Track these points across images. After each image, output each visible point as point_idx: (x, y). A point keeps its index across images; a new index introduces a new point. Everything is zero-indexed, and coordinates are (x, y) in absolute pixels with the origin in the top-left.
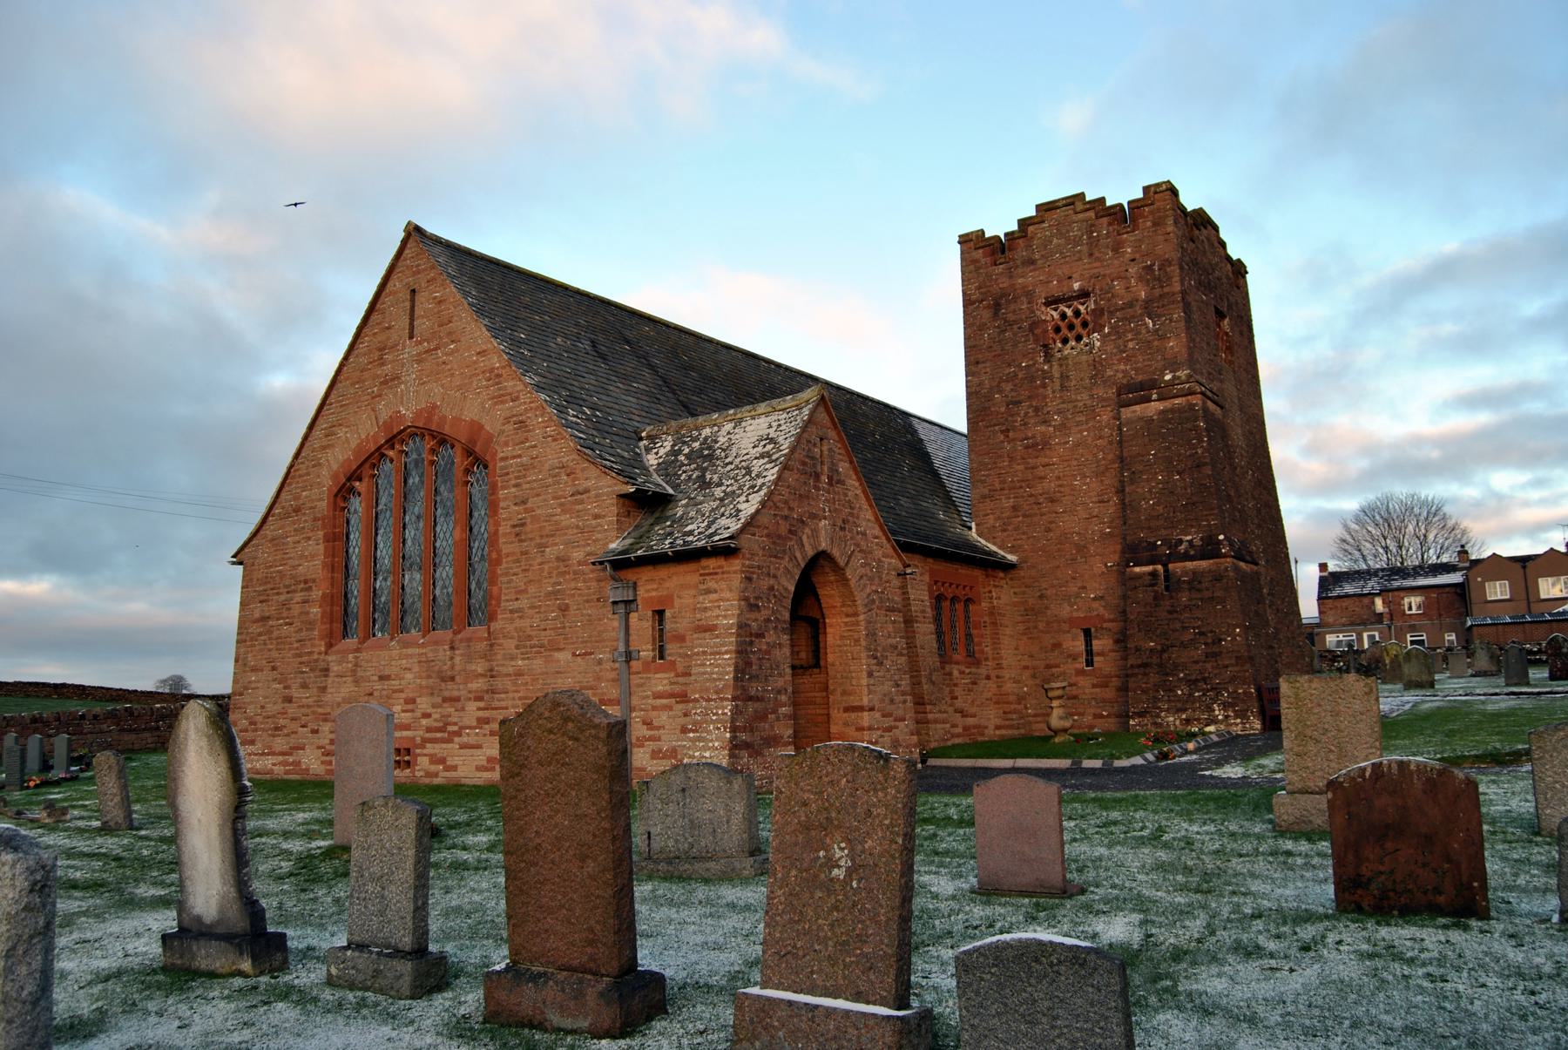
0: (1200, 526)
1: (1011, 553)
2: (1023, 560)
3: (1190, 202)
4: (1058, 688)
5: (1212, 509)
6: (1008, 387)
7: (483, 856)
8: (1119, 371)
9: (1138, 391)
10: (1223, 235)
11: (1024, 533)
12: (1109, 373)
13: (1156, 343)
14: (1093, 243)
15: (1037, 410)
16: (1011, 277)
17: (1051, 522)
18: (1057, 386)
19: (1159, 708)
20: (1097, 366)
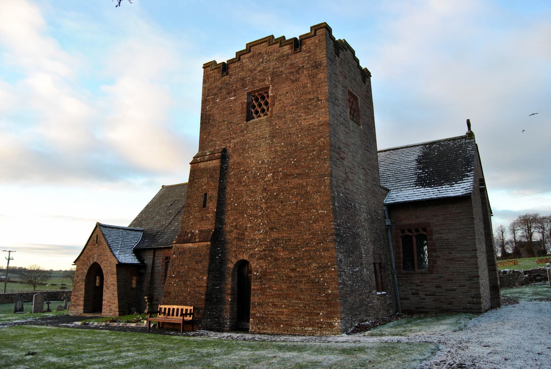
3: (337, 35)
7: (467, 141)
10: (357, 55)
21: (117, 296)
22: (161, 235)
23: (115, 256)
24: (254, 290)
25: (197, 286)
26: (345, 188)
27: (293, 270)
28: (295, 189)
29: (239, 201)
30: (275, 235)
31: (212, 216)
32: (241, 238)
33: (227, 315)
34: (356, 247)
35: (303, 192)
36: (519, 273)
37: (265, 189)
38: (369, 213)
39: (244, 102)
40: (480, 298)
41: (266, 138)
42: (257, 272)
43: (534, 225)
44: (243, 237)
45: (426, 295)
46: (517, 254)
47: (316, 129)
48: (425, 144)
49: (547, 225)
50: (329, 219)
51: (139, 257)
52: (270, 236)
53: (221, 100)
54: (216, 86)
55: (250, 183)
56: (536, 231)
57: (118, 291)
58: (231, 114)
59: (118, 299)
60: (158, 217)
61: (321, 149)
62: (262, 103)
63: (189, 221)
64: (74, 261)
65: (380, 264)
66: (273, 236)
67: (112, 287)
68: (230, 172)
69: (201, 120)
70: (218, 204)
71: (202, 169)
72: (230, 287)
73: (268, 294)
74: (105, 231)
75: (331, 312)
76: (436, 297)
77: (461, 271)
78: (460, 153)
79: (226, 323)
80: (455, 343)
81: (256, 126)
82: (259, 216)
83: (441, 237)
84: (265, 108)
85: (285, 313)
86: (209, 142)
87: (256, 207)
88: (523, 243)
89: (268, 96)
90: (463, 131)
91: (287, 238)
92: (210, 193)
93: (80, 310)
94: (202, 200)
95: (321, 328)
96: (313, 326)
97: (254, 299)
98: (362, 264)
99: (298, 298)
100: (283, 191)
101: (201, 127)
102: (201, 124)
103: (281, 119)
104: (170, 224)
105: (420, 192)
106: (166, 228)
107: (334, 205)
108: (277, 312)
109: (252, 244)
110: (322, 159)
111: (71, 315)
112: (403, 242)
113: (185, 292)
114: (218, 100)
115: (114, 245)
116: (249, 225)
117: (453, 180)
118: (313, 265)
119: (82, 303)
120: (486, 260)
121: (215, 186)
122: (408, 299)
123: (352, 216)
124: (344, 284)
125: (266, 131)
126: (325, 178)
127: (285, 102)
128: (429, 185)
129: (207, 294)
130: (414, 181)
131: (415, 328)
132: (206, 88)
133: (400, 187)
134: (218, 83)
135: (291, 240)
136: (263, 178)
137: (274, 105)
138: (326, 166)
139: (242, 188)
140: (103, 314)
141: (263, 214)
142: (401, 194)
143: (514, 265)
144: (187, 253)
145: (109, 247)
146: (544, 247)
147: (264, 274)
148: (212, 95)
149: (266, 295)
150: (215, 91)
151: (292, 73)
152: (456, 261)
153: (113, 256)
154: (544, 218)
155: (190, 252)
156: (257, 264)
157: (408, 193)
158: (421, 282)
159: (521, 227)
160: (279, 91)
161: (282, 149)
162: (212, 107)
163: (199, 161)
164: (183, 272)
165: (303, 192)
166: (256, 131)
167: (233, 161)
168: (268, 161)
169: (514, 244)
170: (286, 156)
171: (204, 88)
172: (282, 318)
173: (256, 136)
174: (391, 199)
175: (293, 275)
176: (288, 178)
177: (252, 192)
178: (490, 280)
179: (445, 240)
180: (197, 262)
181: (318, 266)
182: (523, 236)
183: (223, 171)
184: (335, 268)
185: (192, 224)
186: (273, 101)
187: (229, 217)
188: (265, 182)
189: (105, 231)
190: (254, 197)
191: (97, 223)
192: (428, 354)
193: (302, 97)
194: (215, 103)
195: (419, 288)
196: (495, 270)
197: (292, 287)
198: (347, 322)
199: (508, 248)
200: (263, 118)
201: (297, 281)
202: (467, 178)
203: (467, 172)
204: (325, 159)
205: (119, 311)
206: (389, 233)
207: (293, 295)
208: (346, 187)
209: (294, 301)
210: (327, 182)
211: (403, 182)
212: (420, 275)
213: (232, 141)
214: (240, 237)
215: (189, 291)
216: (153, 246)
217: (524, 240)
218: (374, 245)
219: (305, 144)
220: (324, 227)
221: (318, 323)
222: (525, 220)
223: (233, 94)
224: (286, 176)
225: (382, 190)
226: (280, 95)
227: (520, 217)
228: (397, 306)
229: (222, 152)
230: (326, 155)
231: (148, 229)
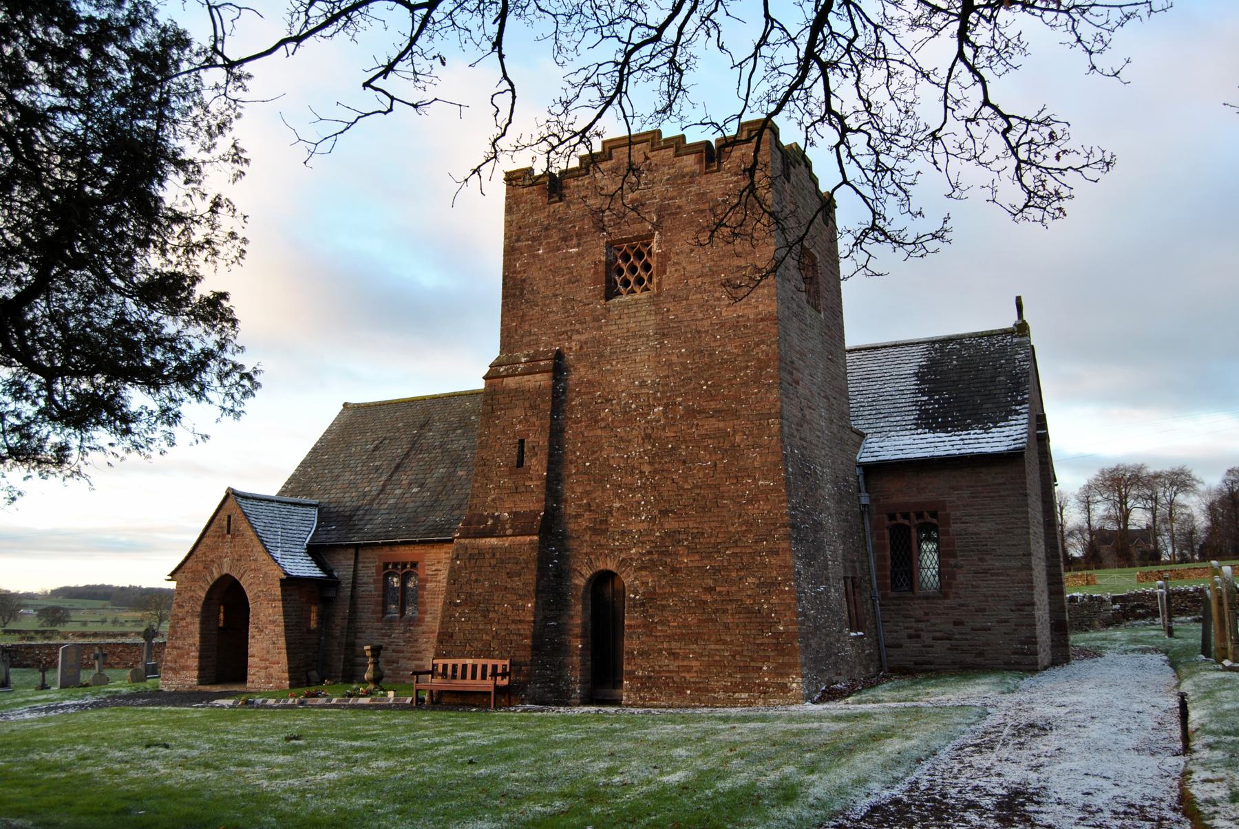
7: (1015, 340)
21: (284, 646)
22: (364, 515)
23: (276, 561)
24: (630, 626)
25: (513, 622)
26: (800, 439)
27: (710, 590)
28: (710, 438)
29: (595, 456)
30: (670, 524)
31: (537, 486)
32: (599, 528)
33: (575, 674)
34: (819, 548)
35: (727, 446)
36: (1101, 601)
37: (648, 437)
38: (836, 484)
39: (600, 261)
40: (1036, 643)
41: (648, 336)
43: (1134, 492)
44: (603, 527)
45: (934, 638)
46: (1093, 559)
47: (751, 326)
48: (932, 342)
49: (1164, 493)
50: (778, 496)
51: (320, 564)
52: (662, 525)
53: (549, 252)
54: (536, 221)
55: (615, 424)
56: (1138, 505)
57: (286, 637)
58: (570, 282)
59: (288, 653)
60: (347, 476)
61: (762, 365)
62: (638, 264)
63: (487, 494)
64: (169, 572)
65: (853, 578)
66: (666, 526)
67: (272, 627)
68: (572, 400)
69: (503, 288)
70: (550, 462)
71: (510, 391)
72: (579, 621)
73: (659, 634)
74: (247, 506)
75: (784, 665)
76: (953, 642)
77: (1000, 593)
78: (1002, 364)
79: (574, 691)
80: (1010, 705)
81: (626, 311)
82: (638, 487)
83: (965, 530)
84: (645, 277)
85: (695, 669)
86: (522, 336)
87: (630, 470)
88: (1107, 534)
89: (650, 253)
90: (1008, 320)
91: (696, 531)
92: (531, 439)
93: (190, 679)
94: (515, 452)
95: (765, 693)
96: (747, 689)
97: (632, 644)
98: (828, 579)
99: (720, 641)
100: (685, 441)
101: (503, 303)
102: (504, 297)
103: (679, 302)
104: (382, 491)
105: (925, 441)
106: (374, 500)
107: (786, 470)
108: (679, 667)
109: (623, 540)
110: (764, 385)
111: (166, 689)
112: (891, 538)
113: (487, 634)
114: (541, 252)
115: (268, 537)
116: (617, 505)
117: (990, 420)
118: (749, 580)
119: (194, 663)
120: (1045, 573)
121: (542, 426)
122: (901, 646)
123: (812, 490)
124: (805, 616)
125: (648, 323)
126: (770, 421)
127: (688, 268)
128: (943, 427)
129: (535, 637)
130: (912, 417)
131: (933, 690)
132: (514, 224)
133: (886, 429)
134: (541, 217)
135: (703, 533)
136: (644, 415)
137: (665, 272)
138: (771, 398)
139: (599, 432)
140: (248, 685)
141: (645, 484)
142: (889, 444)
143: (1087, 584)
144: (487, 556)
145: (262, 541)
146: (1156, 543)
147: (651, 597)
148: (528, 240)
149: (656, 637)
150: (534, 232)
151: (702, 211)
152: (992, 575)
153: (270, 561)
154: (1157, 476)
155: (494, 555)
156: (636, 579)
157: (902, 443)
158: (926, 614)
159: (1105, 496)
160: (674, 246)
161: (681, 360)
162: (528, 263)
163: (505, 373)
164: (480, 594)
165: (727, 446)
166: (626, 320)
167: (578, 377)
168: (652, 381)
169: (1087, 537)
170: (690, 374)
171: (508, 224)
172: (688, 678)
173: (628, 332)
174: (869, 454)
175: (708, 598)
176: (695, 417)
177: (622, 440)
178: (1051, 612)
179: (972, 534)
180: (510, 575)
181: (757, 582)
182: (1109, 518)
183: (557, 397)
184: (790, 586)
185: (493, 500)
186: (661, 263)
187: (572, 488)
188: (648, 422)
189: (247, 506)
190: (626, 450)
191: (229, 489)
192: (975, 719)
193: (722, 263)
194: (534, 256)
195: (921, 625)
196: (1062, 593)
197: (707, 621)
198: (810, 683)
199: (1073, 545)
200: (640, 295)
201: (717, 610)
202: (1015, 417)
203: (1016, 405)
204: (769, 384)
205: (290, 679)
206: (867, 521)
207: (710, 636)
208: (802, 436)
209: (713, 647)
210: (775, 428)
211: (892, 419)
212: (925, 602)
213: (574, 337)
214: (597, 527)
215: (496, 631)
216: (355, 540)
217: (1111, 526)
218: (844, 543)
219: (729, 353)
220: (769, 512)
221: (759, 685)
222: (1113, 479)
223: (575, 241)
224: (691, 413)
225: (854, 435)
226: (677, 254)
227: (1103, 473)
228: (880, 659)
229: (555, 359)
230: (771, 378)
231: (329, 502)
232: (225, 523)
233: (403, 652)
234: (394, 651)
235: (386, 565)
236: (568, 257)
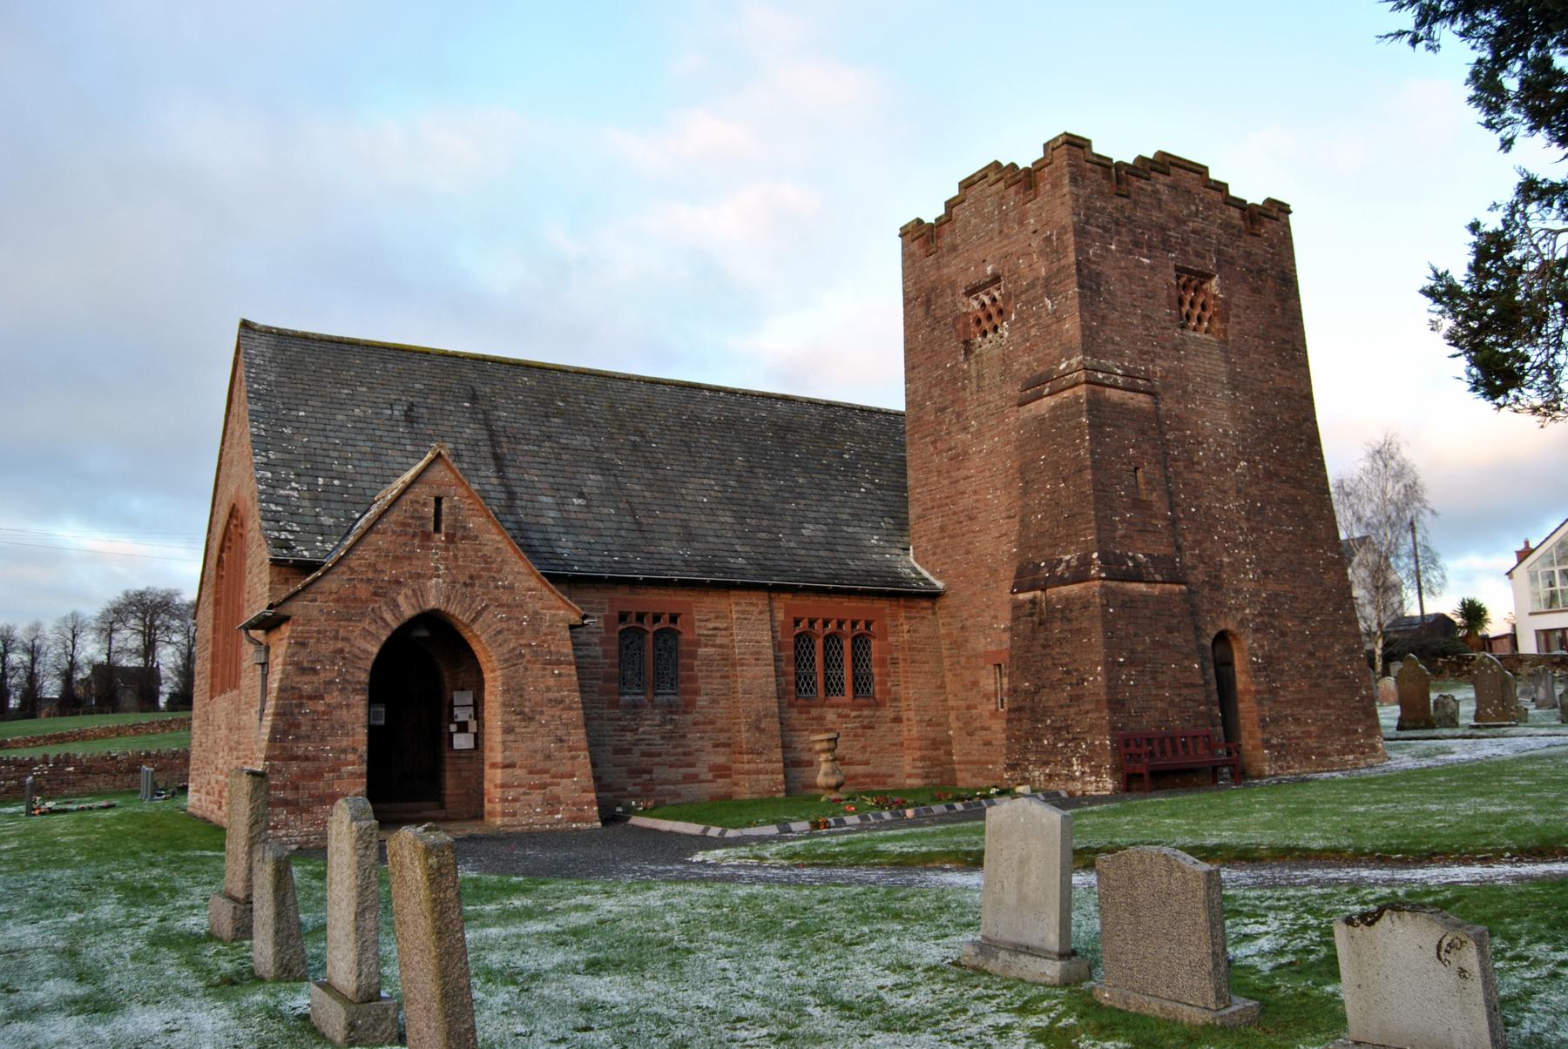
0: (1078, 543)
1: (939, 579)
2: (949, 587)
4: (822, 741)
5: (1090, 522)
6: (936, 392)
8: (1025, 364)
9: (1035, 386)
11: (949, 557)
12: (1016, 367)
13: (1054, 327)
14: (1004, 217)
15: (959, 415)
16: (939, 268)
17: (970, 543)
18: (974, 389)
19: (1028, 760)
20: (1006, 359)
30: (1273, 587)
42: (1257, 657)
96: (1352, 752)
114: (1113, 247)
209: (1323, 711)
227: (127, 595)
232: (430, 510)
233: (659, 755)
234: (643, 754)
235: (623, 617)
236: (1140, 265)
